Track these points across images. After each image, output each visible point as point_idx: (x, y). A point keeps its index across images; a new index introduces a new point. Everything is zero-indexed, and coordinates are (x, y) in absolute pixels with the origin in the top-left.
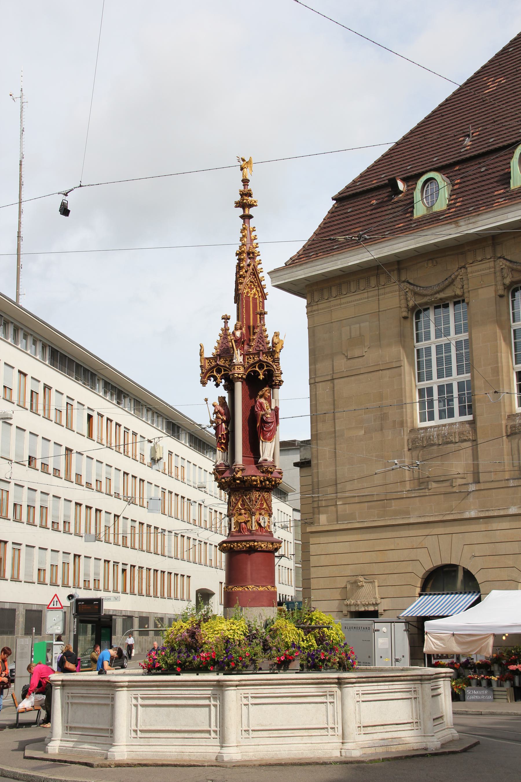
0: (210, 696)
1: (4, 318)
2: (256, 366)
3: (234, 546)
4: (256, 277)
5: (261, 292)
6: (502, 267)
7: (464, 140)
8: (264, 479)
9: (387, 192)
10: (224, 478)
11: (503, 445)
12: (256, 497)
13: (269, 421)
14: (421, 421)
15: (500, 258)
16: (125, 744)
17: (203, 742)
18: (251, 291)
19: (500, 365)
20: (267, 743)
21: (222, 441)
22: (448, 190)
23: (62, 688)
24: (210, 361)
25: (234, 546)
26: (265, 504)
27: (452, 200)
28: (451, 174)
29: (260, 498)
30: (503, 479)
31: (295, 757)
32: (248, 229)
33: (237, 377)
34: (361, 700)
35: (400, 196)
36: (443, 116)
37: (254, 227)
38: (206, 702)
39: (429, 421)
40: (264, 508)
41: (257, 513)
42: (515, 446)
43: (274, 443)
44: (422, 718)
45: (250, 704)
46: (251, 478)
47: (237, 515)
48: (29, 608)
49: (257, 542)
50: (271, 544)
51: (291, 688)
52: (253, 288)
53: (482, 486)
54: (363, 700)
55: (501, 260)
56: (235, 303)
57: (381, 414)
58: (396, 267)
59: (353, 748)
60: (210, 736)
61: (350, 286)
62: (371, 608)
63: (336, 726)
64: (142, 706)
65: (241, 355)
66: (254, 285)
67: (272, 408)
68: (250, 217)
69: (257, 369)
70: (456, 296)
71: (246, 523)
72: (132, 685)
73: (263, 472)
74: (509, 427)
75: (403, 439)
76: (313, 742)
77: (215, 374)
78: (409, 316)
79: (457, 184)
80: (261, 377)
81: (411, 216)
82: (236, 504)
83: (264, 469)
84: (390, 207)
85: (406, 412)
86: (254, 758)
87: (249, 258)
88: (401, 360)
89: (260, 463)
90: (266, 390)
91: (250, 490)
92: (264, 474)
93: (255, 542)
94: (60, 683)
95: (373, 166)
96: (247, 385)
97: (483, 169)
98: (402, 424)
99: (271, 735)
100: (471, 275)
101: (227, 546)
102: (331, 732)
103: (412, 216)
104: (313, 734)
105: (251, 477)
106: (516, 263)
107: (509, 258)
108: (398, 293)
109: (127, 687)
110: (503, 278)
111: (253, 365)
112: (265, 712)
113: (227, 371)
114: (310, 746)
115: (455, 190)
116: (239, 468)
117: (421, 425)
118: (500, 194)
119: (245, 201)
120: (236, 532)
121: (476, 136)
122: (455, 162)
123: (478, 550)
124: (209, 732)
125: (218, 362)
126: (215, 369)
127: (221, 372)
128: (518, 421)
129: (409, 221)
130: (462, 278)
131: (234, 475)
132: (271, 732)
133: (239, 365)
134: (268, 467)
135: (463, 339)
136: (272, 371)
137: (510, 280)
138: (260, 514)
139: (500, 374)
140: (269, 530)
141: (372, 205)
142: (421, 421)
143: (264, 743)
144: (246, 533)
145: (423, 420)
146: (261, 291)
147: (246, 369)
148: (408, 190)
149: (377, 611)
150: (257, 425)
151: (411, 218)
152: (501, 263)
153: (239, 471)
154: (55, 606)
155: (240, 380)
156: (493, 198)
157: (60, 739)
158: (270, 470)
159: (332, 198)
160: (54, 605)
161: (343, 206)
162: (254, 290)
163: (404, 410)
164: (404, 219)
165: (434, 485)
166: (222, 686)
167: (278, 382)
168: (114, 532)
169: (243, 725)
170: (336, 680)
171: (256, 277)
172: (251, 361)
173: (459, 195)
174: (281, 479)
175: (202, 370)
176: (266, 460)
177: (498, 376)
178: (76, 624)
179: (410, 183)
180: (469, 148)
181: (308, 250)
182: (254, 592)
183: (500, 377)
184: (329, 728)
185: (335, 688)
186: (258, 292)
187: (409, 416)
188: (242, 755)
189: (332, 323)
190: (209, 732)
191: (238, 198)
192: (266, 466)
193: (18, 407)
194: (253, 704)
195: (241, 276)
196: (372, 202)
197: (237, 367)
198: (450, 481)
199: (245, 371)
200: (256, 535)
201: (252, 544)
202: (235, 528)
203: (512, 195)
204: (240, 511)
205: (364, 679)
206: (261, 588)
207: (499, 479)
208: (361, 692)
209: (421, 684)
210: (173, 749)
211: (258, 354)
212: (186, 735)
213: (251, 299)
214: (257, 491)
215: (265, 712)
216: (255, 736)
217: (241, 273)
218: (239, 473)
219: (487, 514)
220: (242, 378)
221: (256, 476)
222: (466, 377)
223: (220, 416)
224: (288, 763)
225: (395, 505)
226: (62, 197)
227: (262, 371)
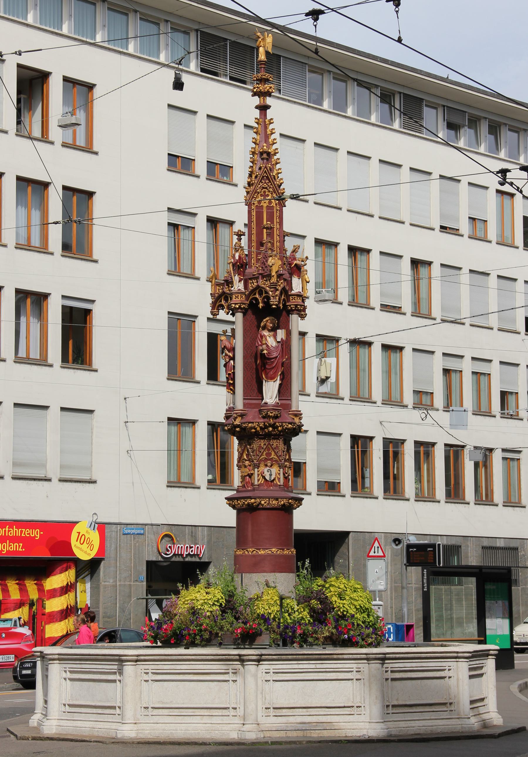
0: (116, 670)
1: (469, 113)
2: (256, 292)
4: (270, 182)
16: (57, 718)
20: (166, 722)
23: (42, 659)
26: (273, 453)
31: (191, 737)
37: (272, 119)
40: (272, 458)
41: (262, 465)
49: (255, 499)
54: (274, 679)
59: (248, 730)
65: (240, 281)
66: (269, 191)
68: (268, 107)
72: (62, 658)
73: (264, 417)
86: (149, 736)
90: (267, 321)
92: (266, 420)
93: (251, 499)
94: (39, 654)
96: (253, 314)
99: (171, 714)
104: (214, 714)
105: (248, 424)
109: (59, 659)
112: (166, 689)
114: (208, 727)
116: (236, 414)
126: (258, 290)
132: (172, 710)
140: (279, 484)
143: (163, 722)
144: (249, 488)
154: (376, 554)
157: (40, 712)
158: (271, 414)
160: (375, 552)
171: (270, 182)
178: (425, 577)
182: (254, 556)
185: (237, 665)
188: (137, 733)
193: (500, 246)
194: (154, 680)
205: (274, 657)
206: (262, 552)
208: (272, 671)
209: (369, 664)
212: (100, 711)
215: (166, 689)
216: (154, 714)
221: (253, 423)
224: (166, 742)
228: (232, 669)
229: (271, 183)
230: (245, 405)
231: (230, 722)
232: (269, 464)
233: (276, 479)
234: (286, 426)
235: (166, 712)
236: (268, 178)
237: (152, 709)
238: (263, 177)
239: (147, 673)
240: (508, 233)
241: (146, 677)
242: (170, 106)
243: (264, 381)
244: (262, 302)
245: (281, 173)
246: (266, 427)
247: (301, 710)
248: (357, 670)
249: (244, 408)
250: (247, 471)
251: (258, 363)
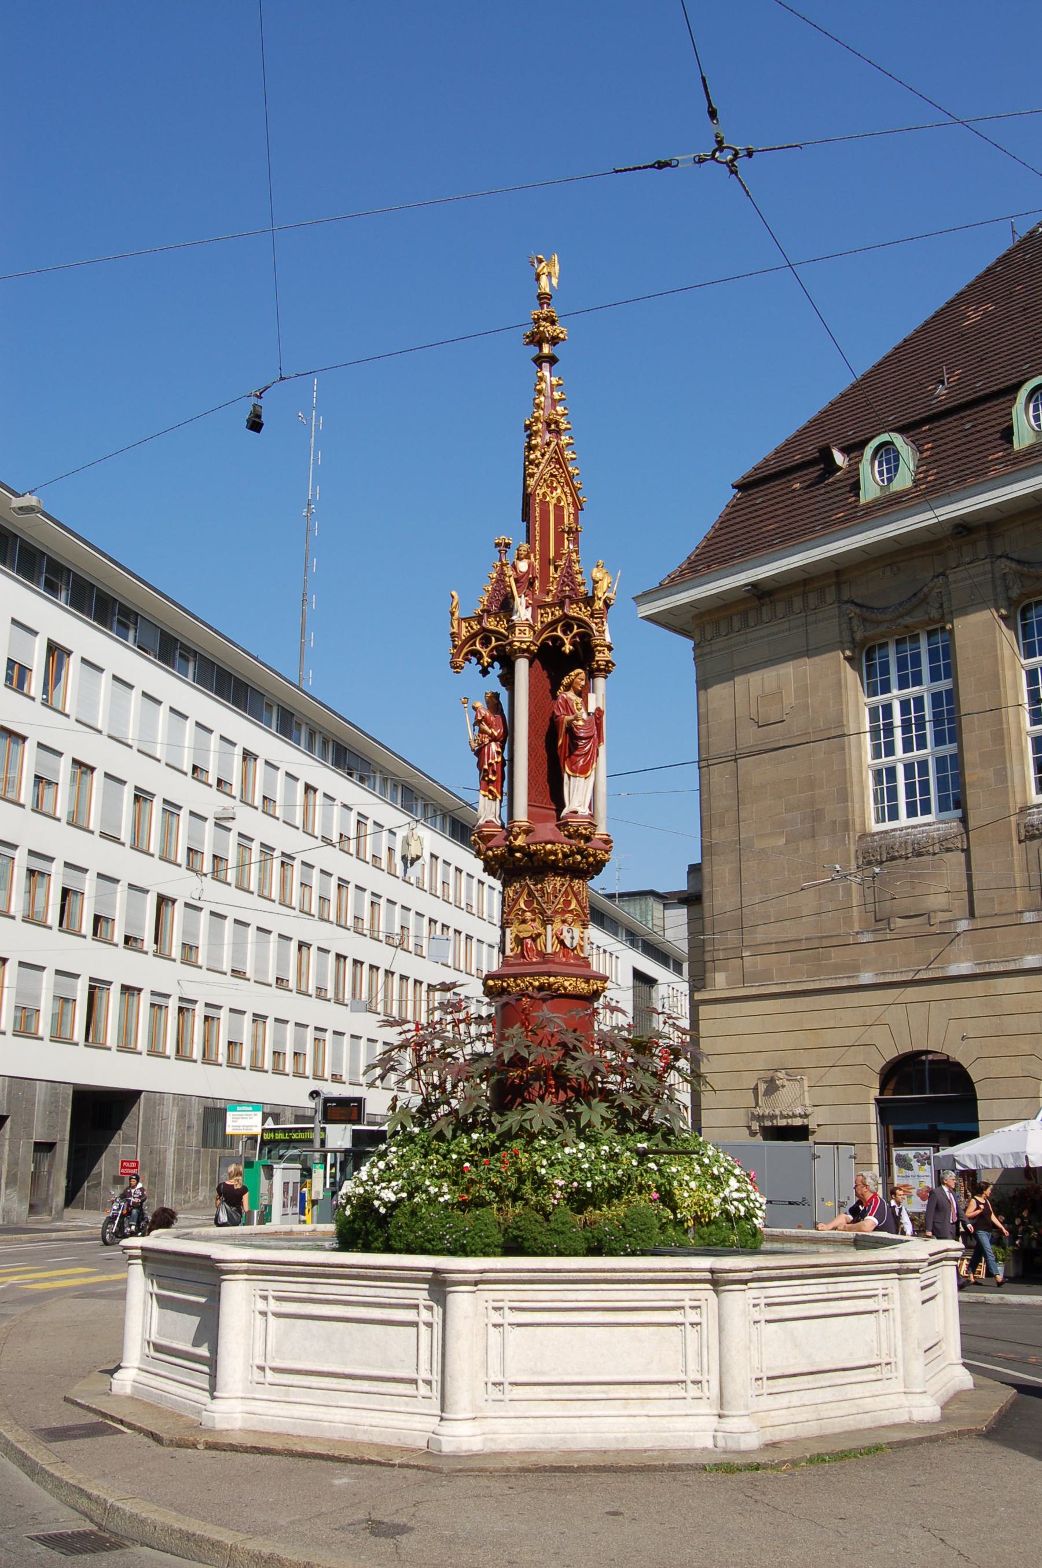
3: (508, 984)
4: (561, 467)
5: (572, 495)
6: (1004, 572)
7: (936, 388)
8: (572, 852)
9: (818, 471)
10: (490, 849)
11: (1012, 856)
12: (554, 888)
13: (582, 735)
14: (877, 822)
15: (1001, 557)
17: (400, 1404)
18: (552, 493)
19: (1005, 726)
21: (491, 776)
22: (914, 459)
24: (469, 624)
25: (508, 984)
27: (921, 473)
28: (918, 437)
29: (563, 889)
30: (1013, 911)
33: (519, 648)
34: (762, 1317)
35: (838, 474)
36: (900, 361)
38: (408, 1315)
39: (922, 815)
40: (571, 910)
41: (558, 919)
42: (1032, 856)
43: (591, 780)
44: (900, 1354)
45: (506, 1325)
46: (543, 847)
47: (516, 923)
48: (210, 1103)
49: (555, 976)
50: (586, 983)
51: (602, 1290)
52: (556, 489)
53: (979, 923)
54: (768, 1318)
55: (1003, 560)
56: (523, 521)
57: (813, 811)
58: (834, 580)
59: (743, 1431)
60: (415, 1393)
61: (761, 614)
62: (798, 1122)
63: (704, 1379)
64: (278, 1315)
65: (527, 607)
66: (559, 483)
67: (589, 711)
69: (559, 633)
70: (931, 621)
71: (534, 938)
72: (258, 1270)
73: (570, 836)
74: (1022, 826)
75: (848, 850)
76: (651, 1413)
77: (478, 647)
78: (856, 656)
79: (927, 450)
80: (568, 648)
81: (856, 501)
82: (516, 901)
83: (571, 830)
84: (822, 491)
85: (853, 806)
87: (550, 432)
88: (843, 726)
89: (565, 818)
90: (578, 675)
91: (542, 873)
93: (550, 976)
94: (138, 1252)
95: (795, 437)
97: (968, 426)
98: (846, 826)
100: (954, 586)
101: (495, 984)
102: (423, 1389)
103: (858, 500)
104: (652, 1395)
105: (543, 844)
106: (1029, 563)
107: (1015, 556)
108: (837, 619)
110: (1007, 589)
111: (553, 624)
113: (502, 640)
115: (925, 458)
117: (875, 827)
118: (997, 459)
119: (541, 329)
120: (516, 956)
121: (954, 381)
122: (922, 419)
123: (971, 1028)
124: (414, 1382)
125: (484, 624)
127: (490, 643)
128: (1035, 819)
129: (853, 508)
130: (941, 592)
131: (511, 842)
134: (580, 826)
135: (943, 689)
137: (1018, 592)
138: (564, 922)
139: (1006, 740)
141: (794, 490)
142: (877, 822)
144: (534, 960)
145: (880, 819)
146: (571, 493)
147: (537, 635)
148: (850, 465)
149: (807, 1126)
150: (557, 742)
151: (856, 504)
152: (1005, 566)
153: (520, 834)
155: (526, 654)
156: (986, 465)
158: (584, 832)
159: (732, 485)
161: (750, 495)
162: (559, 491)
163: (850, 804)
164: (845, 506)
165: (900, 922)
166: (445, 1283)
167: (604, 663)
168: (415, 998)
169: (490, 1372)
170: (708, 1276)
171: (561, 467)
173: (932, 466)
174: (607, 852)
175: (454, 641)
176: (576, 812)
177: (1003, 744)
179: (852, 455)
180: (943, 397)
181: (695, 562)
183: (1006, 746)
184: (689, 1382)
185: (705, 1292)
186: (566, 496)
187: (857, 813)
189: (733, 671)
190: (414, 1382)
194: (514, 1324)
195: (532, 462)
196: (794, 486)
198: (926, 915)
199: (537, 637)
200: (553, 962)
201: (543, 979)
202: (512, 950)
203: (1016, 458)
207: (1006, 912)
208: (763, 1301)
210: (339, 1416)
211: (561, 605)
212: (366, 1386)
213: (551, 508)
214: (557, 874)
217: (532, 457)
218: (520, 837)
219: (987, 969)
220: (528, 650)
221: (553, 843)
222: (949, 749)
223: (486, 727)
225: (836, 956)
226: (254, 400)
227: (569, 637)
228: (690, 1300)
230: (530, 816)
231: (689, 1412)
232: (570, 920)
233: (578, 948)
234: (601, 856)
235: (541, 1392)
236: (558, 462)
237: (510, 1387)
238: (552, 458)
239: (496, 1309)
240: (39, 906)
241: (496, 1318)
242: (14, 622)
243: (566, 776)
246: (572, 854)
247: (806, 1378)
248: (884, 1292)
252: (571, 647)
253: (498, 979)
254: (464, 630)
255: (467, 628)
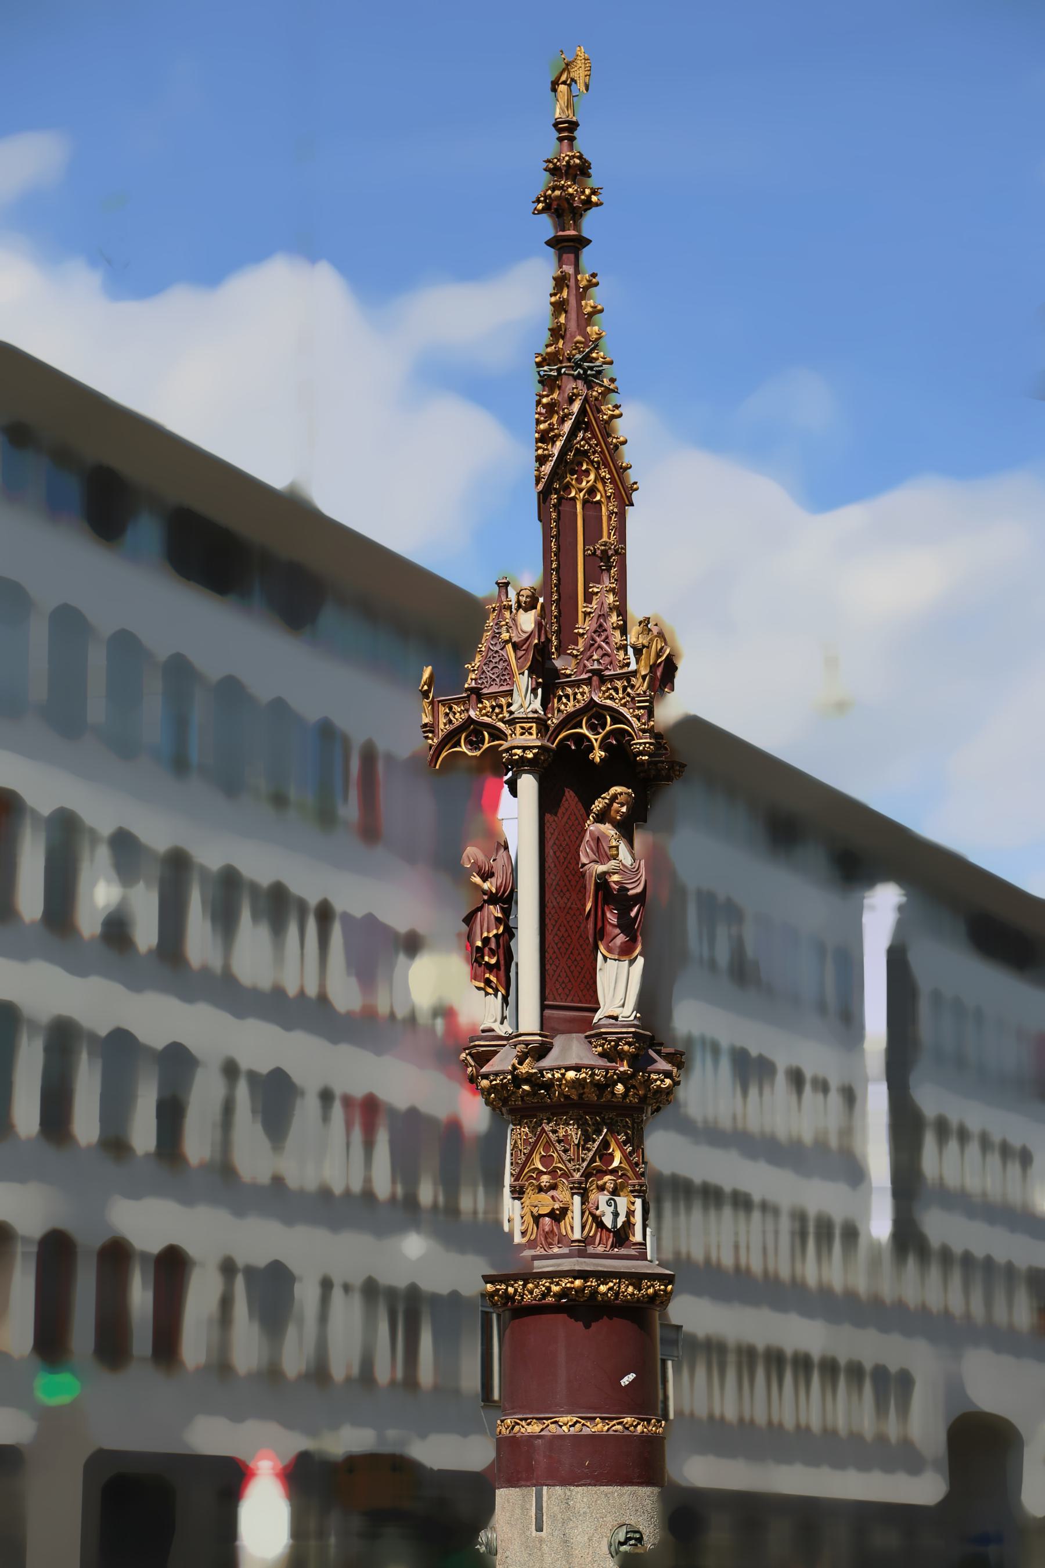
5: (613, 481)
10: (485, 1076)
32: (572, 283)
52: (587, 472)
68: (581, 242)
80: (598, 755)
90: (614, 798)
105: (563, 1071)
127: (483, 742)
133: (527, 720)
134: (620, 1039)
136: (630, 735)
146: (612, 478)
150: (585, 905)
162: (592, 477)
172: (566, 705)
191: (540, 182)
192: (610, 1037)
197: (522, 728)
204: (537, 1179)
227: (600, 737)
229: (597, 439)
232: (610, 1186)
234: (658, 1083)
244: (600, 748)
245: (620, 416)
249: (542, 1030)
250: (545, 1203)
251: (588, 908)
252: (603, 753)
253: (501, 1282)
254: (443, 720)
255: (447, 714)
